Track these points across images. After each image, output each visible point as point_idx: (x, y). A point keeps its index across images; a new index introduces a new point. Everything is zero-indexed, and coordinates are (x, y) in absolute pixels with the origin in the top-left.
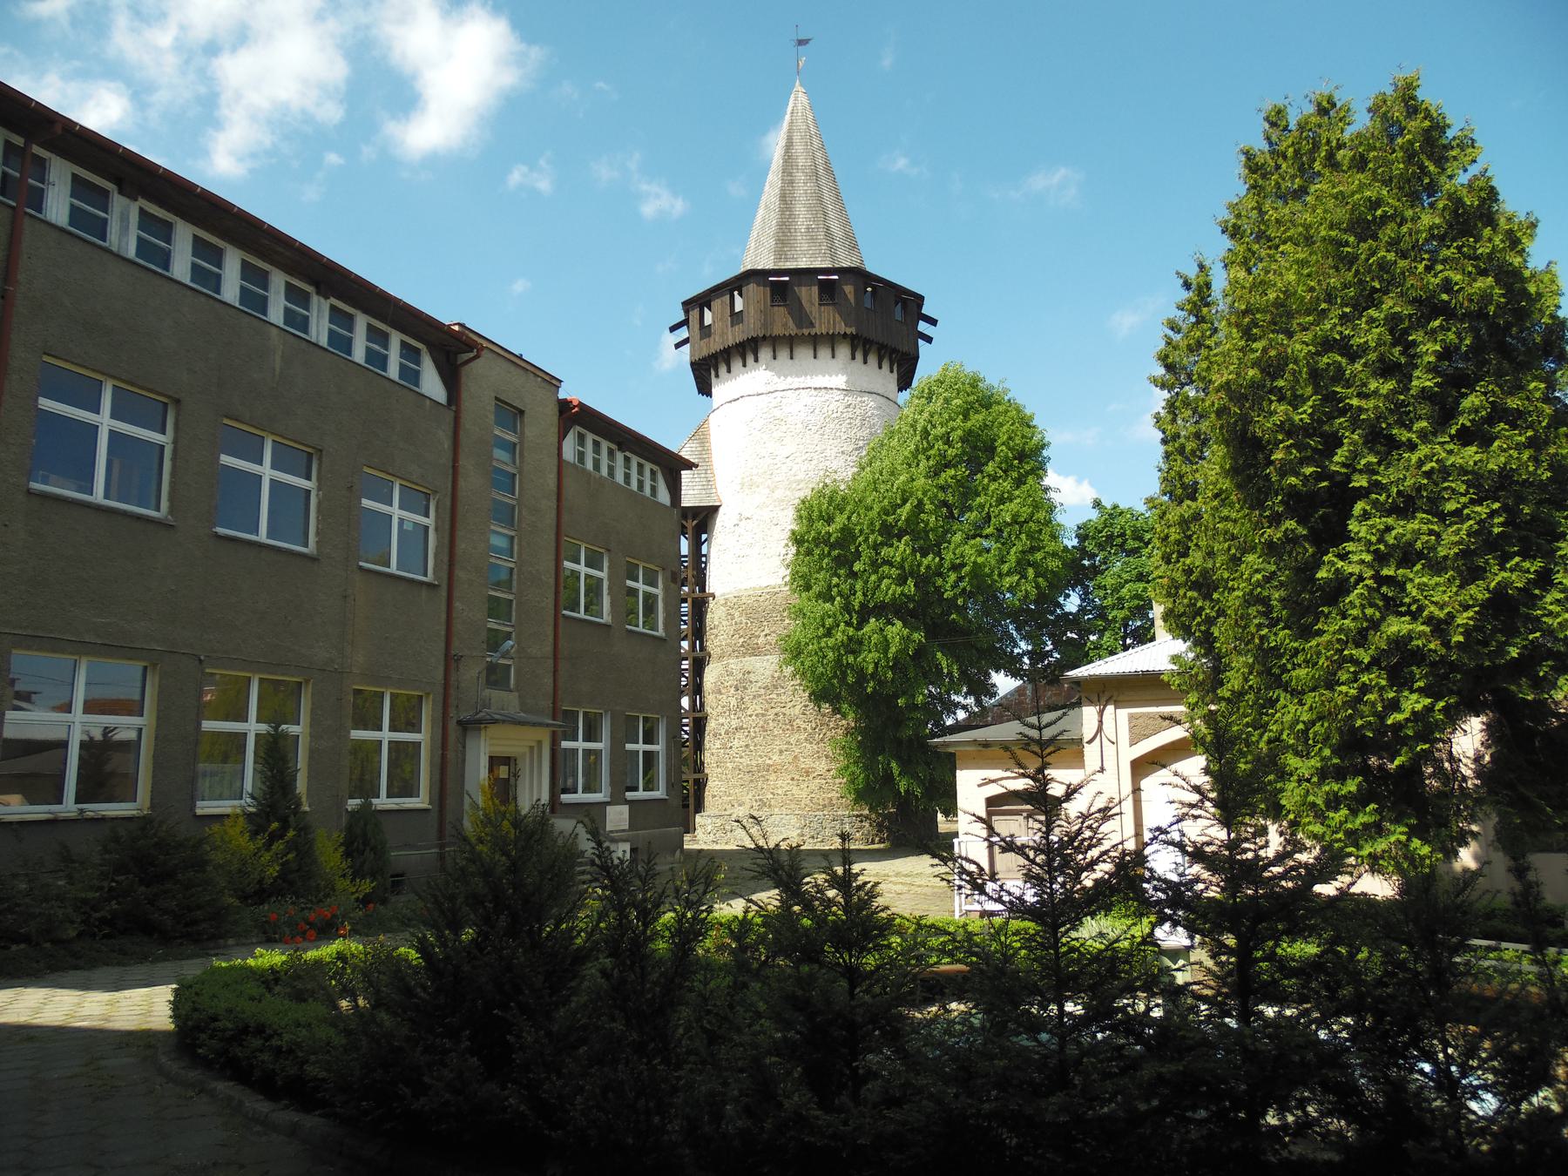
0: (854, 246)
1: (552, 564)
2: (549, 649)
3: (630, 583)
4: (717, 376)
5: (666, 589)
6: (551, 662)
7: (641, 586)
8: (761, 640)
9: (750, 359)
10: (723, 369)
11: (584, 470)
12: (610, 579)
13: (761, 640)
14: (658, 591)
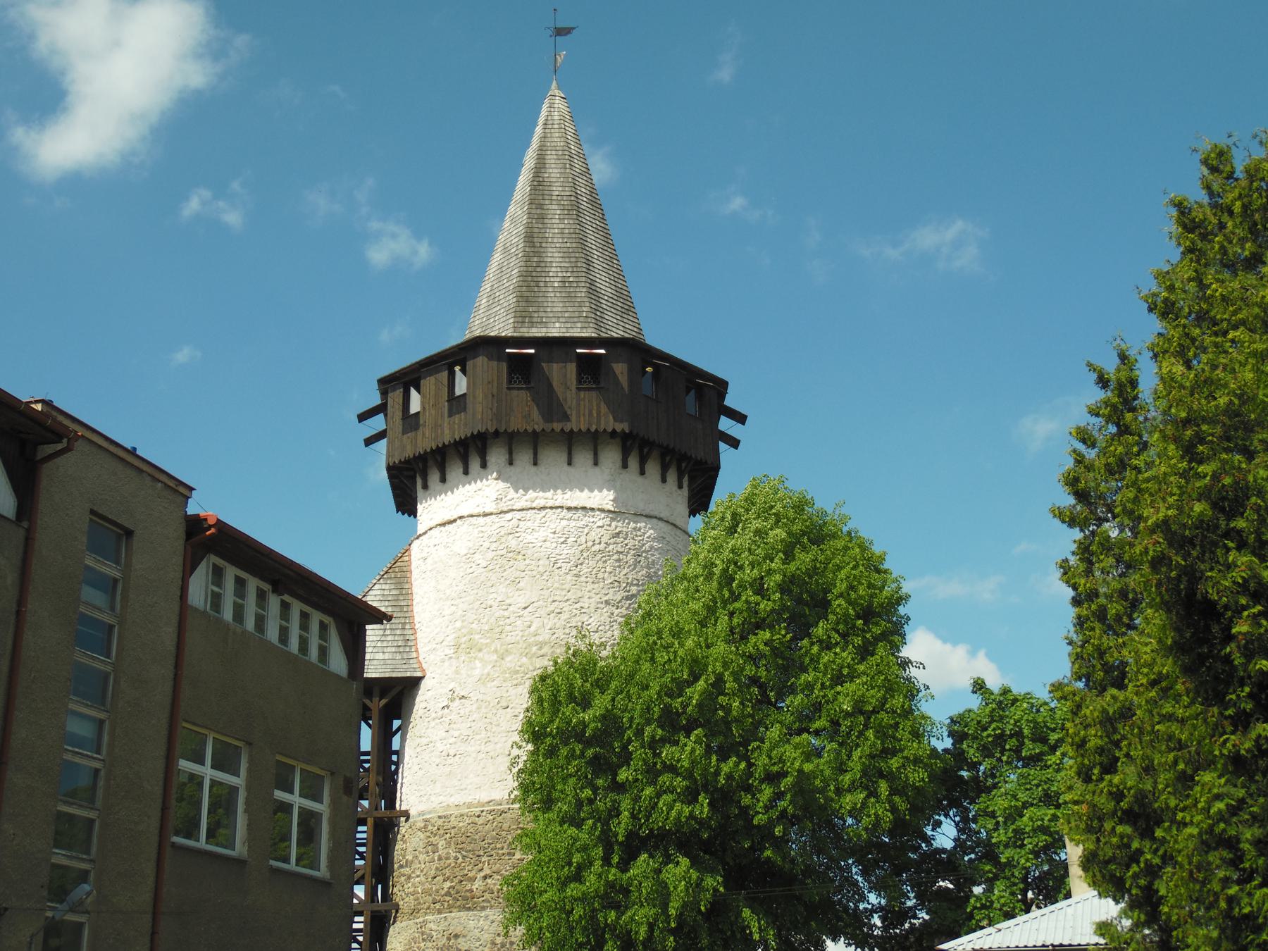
0: (628, 309)
1: (160, 765)
2: (146, 896)
3: (279, 795)
4: (425, 487)
5: (334, 804)
6: (149, 917)
7: (296, 800)
8: (477, 885)
9: (475, 464)
10: (434, 477)
11: (219, 621)
12: (249, 788)
13: (477, 885)
14: (321, 808)
